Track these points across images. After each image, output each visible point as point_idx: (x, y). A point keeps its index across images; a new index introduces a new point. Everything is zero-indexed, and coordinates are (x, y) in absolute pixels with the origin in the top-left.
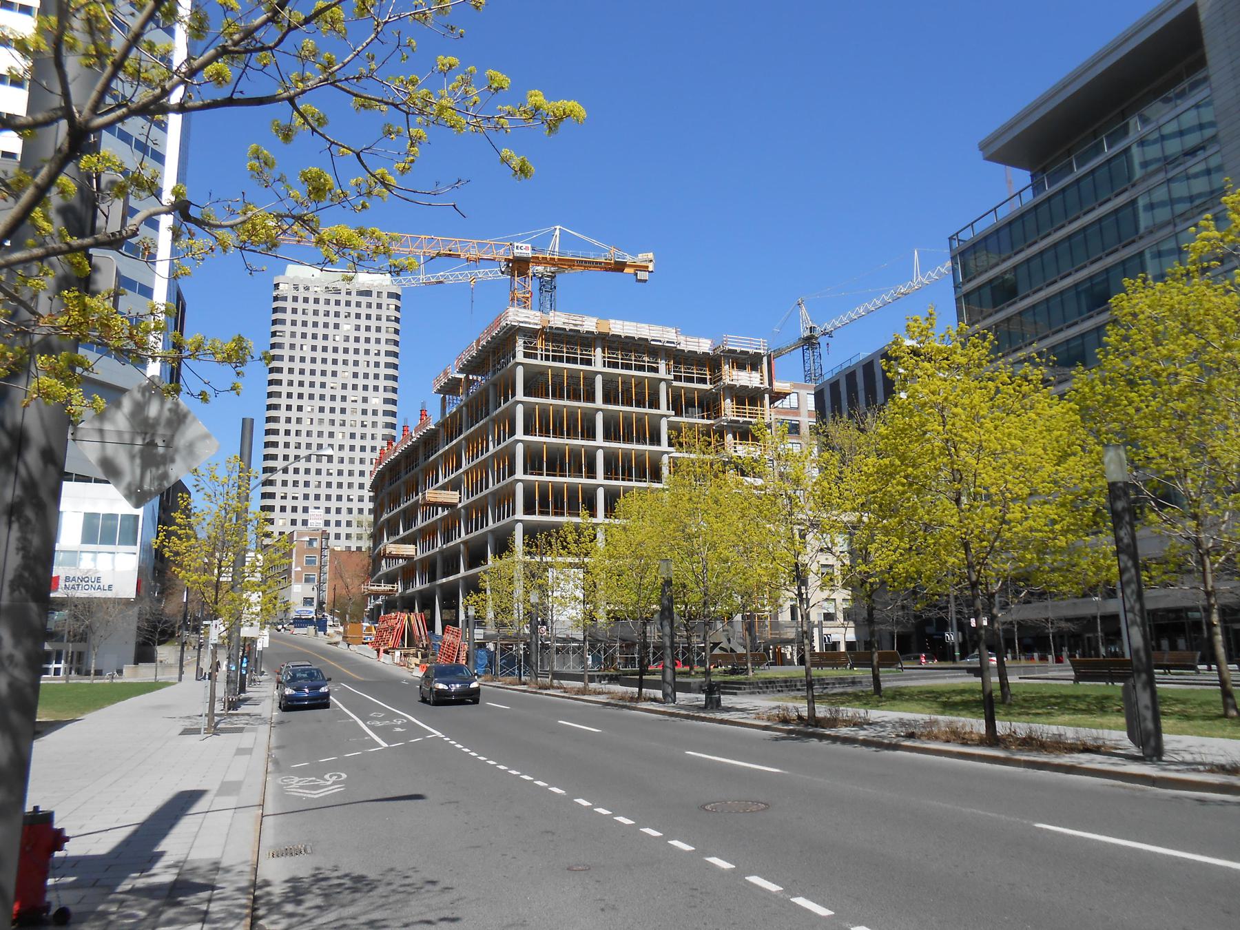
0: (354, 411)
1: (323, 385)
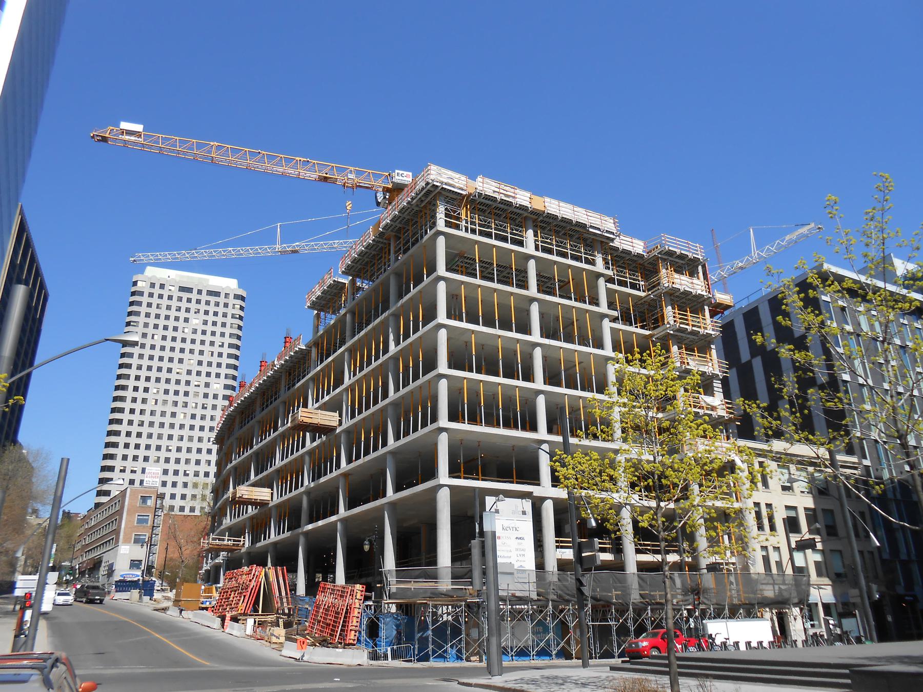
0: (196, 394)
1: (170, 370)
